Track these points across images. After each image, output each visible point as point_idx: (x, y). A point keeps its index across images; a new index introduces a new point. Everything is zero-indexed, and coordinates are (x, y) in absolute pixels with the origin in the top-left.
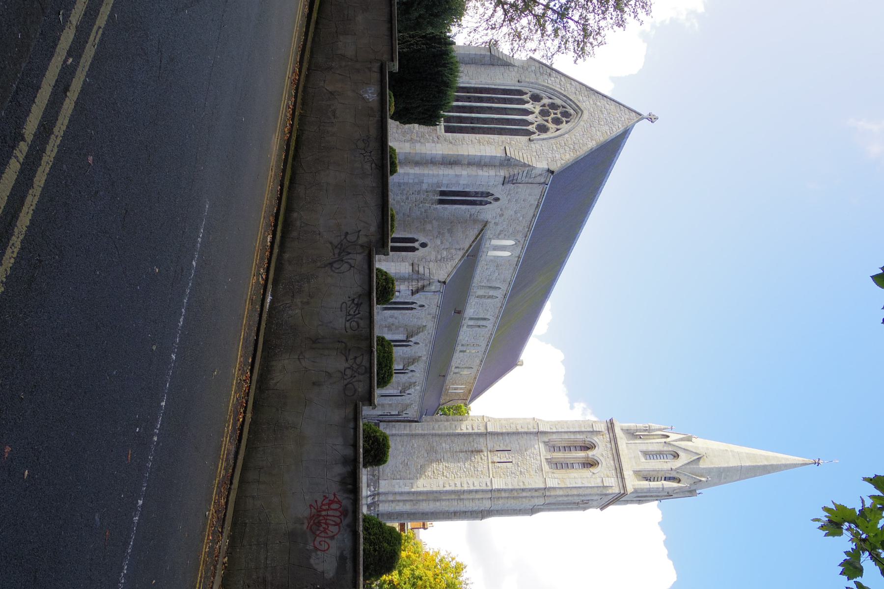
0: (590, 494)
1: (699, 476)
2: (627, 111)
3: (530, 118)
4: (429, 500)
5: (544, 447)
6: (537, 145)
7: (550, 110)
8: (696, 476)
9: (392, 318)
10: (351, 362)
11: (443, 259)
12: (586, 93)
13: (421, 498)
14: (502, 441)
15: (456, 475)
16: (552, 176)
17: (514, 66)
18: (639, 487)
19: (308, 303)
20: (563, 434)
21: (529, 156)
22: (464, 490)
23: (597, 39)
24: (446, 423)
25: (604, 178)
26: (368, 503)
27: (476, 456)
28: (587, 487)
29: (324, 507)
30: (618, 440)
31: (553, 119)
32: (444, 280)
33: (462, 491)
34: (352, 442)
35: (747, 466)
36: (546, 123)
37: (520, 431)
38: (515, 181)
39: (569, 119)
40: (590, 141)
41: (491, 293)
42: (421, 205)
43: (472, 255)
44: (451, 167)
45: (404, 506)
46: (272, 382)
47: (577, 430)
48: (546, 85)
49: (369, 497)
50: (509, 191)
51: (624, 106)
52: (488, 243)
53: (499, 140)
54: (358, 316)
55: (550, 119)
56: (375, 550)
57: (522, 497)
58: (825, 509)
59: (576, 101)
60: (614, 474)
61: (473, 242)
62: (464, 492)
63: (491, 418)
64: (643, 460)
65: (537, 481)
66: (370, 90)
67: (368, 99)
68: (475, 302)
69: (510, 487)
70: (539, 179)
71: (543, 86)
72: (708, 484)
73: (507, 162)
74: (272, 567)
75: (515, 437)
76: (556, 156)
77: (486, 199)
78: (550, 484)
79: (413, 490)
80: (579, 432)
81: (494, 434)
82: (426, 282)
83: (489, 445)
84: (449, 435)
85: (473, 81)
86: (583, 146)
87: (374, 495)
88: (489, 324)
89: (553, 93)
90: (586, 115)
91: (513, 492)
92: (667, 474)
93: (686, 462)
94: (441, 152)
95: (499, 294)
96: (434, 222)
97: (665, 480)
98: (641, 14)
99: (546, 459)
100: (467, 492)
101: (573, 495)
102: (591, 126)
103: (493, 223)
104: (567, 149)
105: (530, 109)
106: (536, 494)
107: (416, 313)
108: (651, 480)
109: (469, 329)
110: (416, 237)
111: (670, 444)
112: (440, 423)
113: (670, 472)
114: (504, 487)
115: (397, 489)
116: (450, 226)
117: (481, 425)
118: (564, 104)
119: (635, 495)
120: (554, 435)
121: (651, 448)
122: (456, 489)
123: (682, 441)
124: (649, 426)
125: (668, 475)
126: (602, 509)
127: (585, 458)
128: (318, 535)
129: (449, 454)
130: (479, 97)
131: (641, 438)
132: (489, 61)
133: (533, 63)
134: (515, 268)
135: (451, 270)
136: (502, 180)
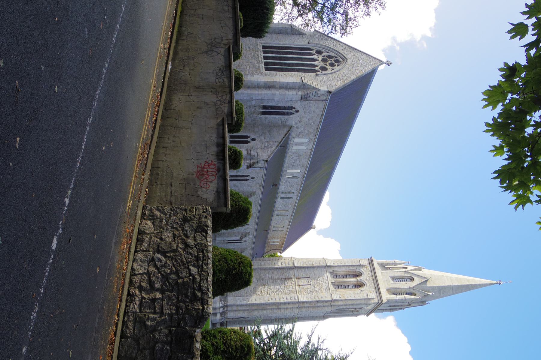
0: (360, 304)
1: (427, 292)
2: (373, 59)
3: (316, 63)
4: (259, 310)
5: (331, 276)
6: (321, 78)
7: (328, 59)
8: (425, 291)
9: (235, 186)
10: (219, 98)
11: (265, 148)
12: (349, 50)
13: (254, 308)
14: (304, 272)
15: (275, 294)
16: (330, 95)
17: (305, 35)
18: (390, 299)
19: (193, 70)
20: (342, 267)
21: (316, 83)
22: (281, 302)
23: (354, 24)
24: (268, 262)
25: (361, 102)
26: (221, 311)
27: (288, 282)
28: (358, 299)
29: (205, 167)
30: (376, 270)
31: (329, 64)
32: (266, 160)
33: (280, 303)
34: (221, 136)
35: (456, 285)
36: (326, 66)
37: (315, 265)
38: (308, 99)
39: (339, 64)
40: (352, 75)
42: (251, 115)
43: (283, 146)
44: (270, 90)
45: (244, 314)
46: (173, 107)
47: (351, 264)
48: (325, 45)
49: (221, 308)
50: (305, 106)
51: (372, 56)
52: (293, 140)
53: (298, 75)
54: (223, 76)
55: (328, 63)
56: (236, 205)
57: (318, 307)
58: (500, 70)
59: (343, 54)
60: (374, 291)
61: (283, 138)
62: (281, 304)
63: (297, 258)
64: (392, 282)
65: (326, 296)
68: (286, 181)
69: (310, 300)
70: (323, 97)
71: (323, 45)
72: (433, 297)
73: (303, 86)
74: (175, 195)
75: (312, 270)
76: (332, 84)
77: (291, 111)
78: (335, 298)
79: (249, 303)
80: (351, 266)
81: (299, 268)
82: (255, 161)
83: (296, 275)
84: (271, 269)
85: (281, 43)
86: (348, 78)
88: (294, 196)
89: (329, 49)
90: (349, 61)
91: (312, 303)
92: (407, 291)
93: (419, 283)
94: (263, 80)
96: (260, 126)
97: (406, 294)
98: (380, 9)
99: (332, 283)
100: (283, 304)
101: (349, 305)
102: (352, 67)
103: (295, 127)
104: (339, 80)
105: (316, 58)
106: (327, 304)
107: (250, 183)
108: (398, 294)
109: (281, 200)
110: (248, 135)
111: (408, 272)
112: (265, 261)
113: (409, 289)
114: (306, 300)
115: (239, 303)
116: (270, 128)
117: (290, 262)
118: (336, 55)
119: (388, 305)
120: (336, 268)
121: (396, 275)
122: (276, 302)
123: (415, 270)
124: (395, 261)
125: (408, 292)
126: (368, 315)
127: (356, 281)
128: (202, 181)
129: (271, 281)
131: (390, 269)
132: (291, 32)
133: (316, 33)
134: (309, 157)
136: (300, 97)
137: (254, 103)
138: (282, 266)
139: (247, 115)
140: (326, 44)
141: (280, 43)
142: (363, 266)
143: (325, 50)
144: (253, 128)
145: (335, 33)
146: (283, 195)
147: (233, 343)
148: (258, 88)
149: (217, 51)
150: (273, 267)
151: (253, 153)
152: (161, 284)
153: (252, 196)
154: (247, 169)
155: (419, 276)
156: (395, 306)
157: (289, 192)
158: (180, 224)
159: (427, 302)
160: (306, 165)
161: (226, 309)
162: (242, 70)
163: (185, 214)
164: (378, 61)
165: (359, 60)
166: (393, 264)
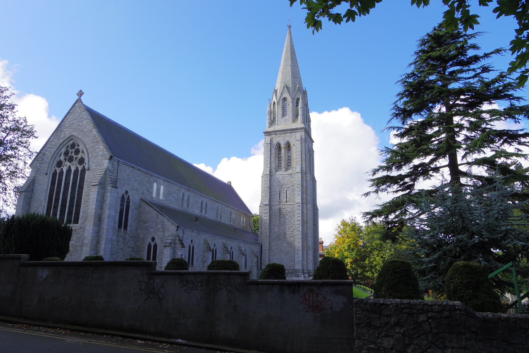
0: (305, 148)
2: (74, 108)
3: (73, 169)
8: (296, 89)
17: (35, 177)
18: (301, 120)
20: (271, 161)
21: (99, 171)
24: (263, 229)
28: (301, 149)
29: (308, 303)
30: (275, 130)
31: (75, 154)
38: (116, 181)
39: (77, 144)
41: (186, 198)
42: (127, 240)
48: (51, 157)
51: (70, 110)
52: (154, 199)
55: (75, 156)
59: (64, 139)
64: (287, 117)
65: (297, 177)
66: (40, 274)
67: (47, 275)
69: (300, 192)
71: (51, 159)
72: (300, 83)
73: (102, 185)
77: (126, 199)
78: (299, 169)
79: (301, 249)
82: (177, 238)
87: (304, 272)
88: (205, 200)
89: (57, 153)
90: (75, 134)
94: (92, 227)
95: (187, 194)
96: (139, 232)
97: (298, 106)
102: (82, 131)
105: (67, 168)
106: (304, 178)
110: (147, 244)
112: (263, 232)
115: (300, 259)
118: (65, 147)
120: (272, 166)
127: (285, 149)
129: (281, 228)
130: (55, 201)
134: (171, 183)
135: (170, 223)
136: (114, 189)
137: (115, 238)
138: (268, 216)
139: (126, 245)
140: (50, 156)
141: (43, 205)
142: (271, 141)
143: (57, 157)
144: (140, 239)
145: (28, 144)
146: (204, 211)
147: (465, 281)
148: (100, 233)
149: (158, 288)
150: (269, 225)
151: (168, 240)
152: (437, 349)
153: (208, 243)
154: (184, 247)
155: (282, 92)
156: (307, 117)
157: (202, 203)
158: (374, 330)
159: (304, 90)
160: (178, 187)
161: (306, 271)
162: (74, 249)
163: (363, 325)
164: (76, 104)
165: (75, 123)
166: (271, 114)
